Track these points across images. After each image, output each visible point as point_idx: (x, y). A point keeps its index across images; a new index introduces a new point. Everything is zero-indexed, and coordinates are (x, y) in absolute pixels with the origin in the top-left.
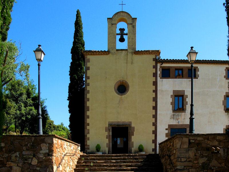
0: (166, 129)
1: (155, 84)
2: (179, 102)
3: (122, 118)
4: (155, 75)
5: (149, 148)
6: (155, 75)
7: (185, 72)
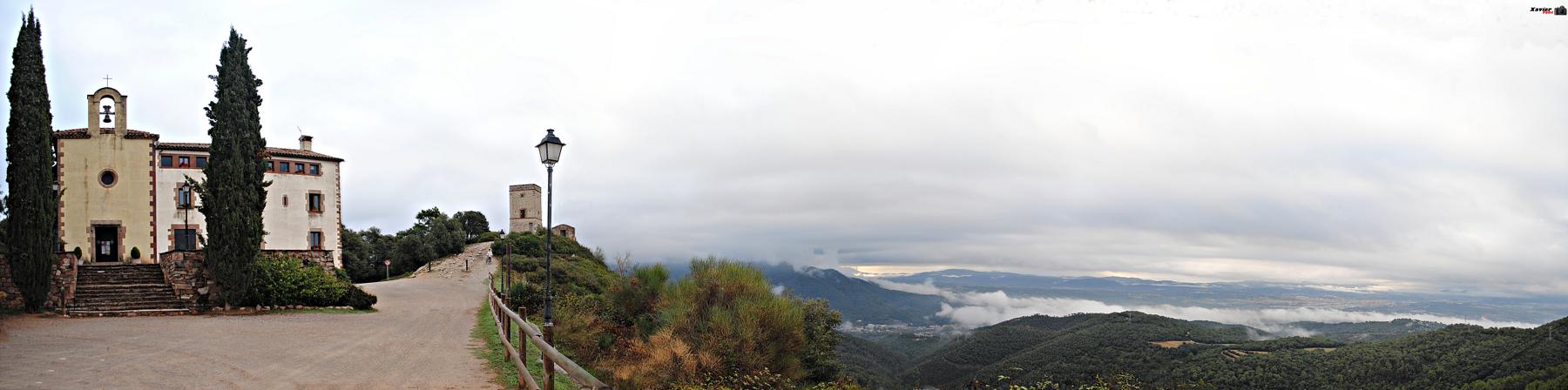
0: (319, 234)
1: (153, 174)
2: (315, 202)
3: (108, 218)
4: (152, 163)
5: (146, 256)
6: (152, 163)
7: (193, 161)
